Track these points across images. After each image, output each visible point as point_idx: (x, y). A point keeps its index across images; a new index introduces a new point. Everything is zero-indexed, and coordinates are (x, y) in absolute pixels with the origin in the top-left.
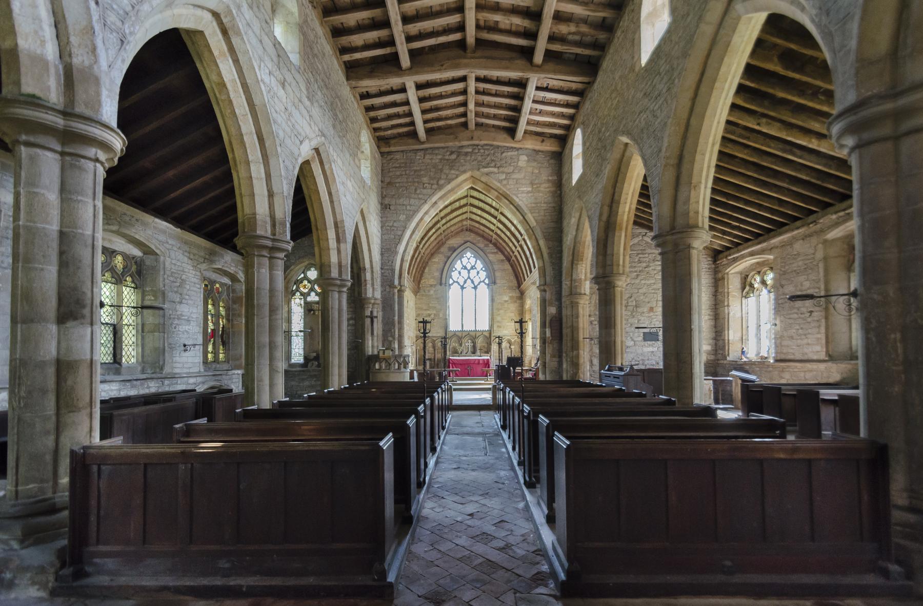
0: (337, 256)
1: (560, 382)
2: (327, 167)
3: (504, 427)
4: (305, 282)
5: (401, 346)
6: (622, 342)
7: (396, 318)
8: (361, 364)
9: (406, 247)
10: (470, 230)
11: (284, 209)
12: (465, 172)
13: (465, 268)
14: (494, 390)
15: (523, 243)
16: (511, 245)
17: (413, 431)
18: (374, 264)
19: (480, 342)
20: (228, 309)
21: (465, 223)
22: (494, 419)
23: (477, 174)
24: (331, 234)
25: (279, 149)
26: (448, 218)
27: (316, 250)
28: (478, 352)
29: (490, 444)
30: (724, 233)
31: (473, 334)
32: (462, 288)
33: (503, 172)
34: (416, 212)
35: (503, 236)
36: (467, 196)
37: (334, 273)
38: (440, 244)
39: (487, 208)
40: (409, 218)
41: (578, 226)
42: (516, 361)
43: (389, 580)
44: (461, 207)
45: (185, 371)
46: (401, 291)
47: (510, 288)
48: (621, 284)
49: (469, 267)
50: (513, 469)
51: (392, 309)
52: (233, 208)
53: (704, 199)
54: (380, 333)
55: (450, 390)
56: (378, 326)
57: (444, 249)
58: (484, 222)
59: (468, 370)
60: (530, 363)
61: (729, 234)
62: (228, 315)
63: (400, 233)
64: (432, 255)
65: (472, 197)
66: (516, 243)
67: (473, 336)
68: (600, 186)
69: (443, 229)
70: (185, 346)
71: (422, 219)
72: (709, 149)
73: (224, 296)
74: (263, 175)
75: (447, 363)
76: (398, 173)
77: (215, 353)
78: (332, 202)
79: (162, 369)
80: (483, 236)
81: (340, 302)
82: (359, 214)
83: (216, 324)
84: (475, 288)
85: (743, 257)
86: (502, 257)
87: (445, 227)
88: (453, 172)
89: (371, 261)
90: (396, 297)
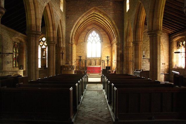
0: (53, 34)
1: (123, 75)
2: (51, 8)
3: (104, 88)
4: (42, 42)
5: (72, 63)
6: (141, 62)
7: (70, 53)
8: (59, 68)
9: (73, 31)
10: (95, 24)
11: (40, 23)
12: (92, 7)
13: (93, 36)
14: (102, 77)
15: (112, 29)
16: (108, 29)
17: (77, 87)
18: (63, 37)
19: (97, 61)
20: (19, 51)
21: (93, 22)
22: (101, 86)
23: (96, 8)
24: (51, 28)
25: (39, 6)
26: (87, 20)
27: (46, 33)
28: (97, 65)
29: (99, 93)
30: (171, 29)
31: (95, 59)
32: (92, 43)
33: (105, 7)
34: (77, 19)
35: (105, 26)
36: (93, 14)
37: (52, 40)
38: (85, 29)
39: (100, 17)
40: (75, 22)
41: (128, 25)
42: (108, 68)
43: (72, 121)
44: (91, 17)
45: (8, 70)
46: (72, 45)
47: (108, 43)
48: (140, 44)
49: (94, 36)
50: (106, 100)
51: (69, 51)
52: (25, 23)
53: (161, 22)
54: (65, 58)
55: (87, 77)
56: (64, 56)
57: (86, 30)
58: (99, 21)
59: (94, 70)
60: (114, 68)
61: (173, 29)
62: (19, 52)
63: (72, 26)
64: (82, 32)
65: (95, 14)
66: (109, 29)
67: (95, 59)
68: (134, 14)
69: (85, 24)
70: (8, 62)
71: (79, 21)
72: (161, 8)
73: (18, 47)
74: (34, 13)
75: (86, 68)
76: (71, 7)
77: (16, 64)
78: (52, 18)
79: (2, 69)
80: (99, 26)
81: (53, 49)
82: (59, 21)
83: (16, 55)
84: (96, 43)
85: (177, 36)
86: (105, 33)
87: (86, 23)
88: (89, 7)
89: (62, 35)
90: (70, 47)
